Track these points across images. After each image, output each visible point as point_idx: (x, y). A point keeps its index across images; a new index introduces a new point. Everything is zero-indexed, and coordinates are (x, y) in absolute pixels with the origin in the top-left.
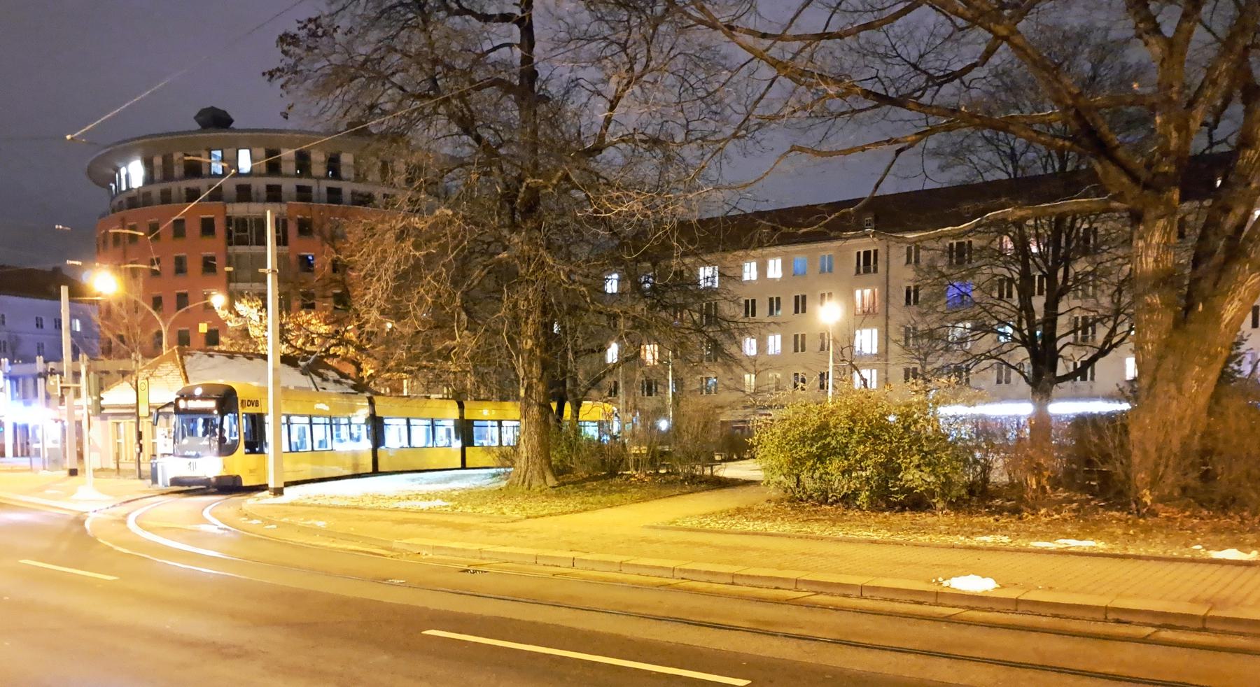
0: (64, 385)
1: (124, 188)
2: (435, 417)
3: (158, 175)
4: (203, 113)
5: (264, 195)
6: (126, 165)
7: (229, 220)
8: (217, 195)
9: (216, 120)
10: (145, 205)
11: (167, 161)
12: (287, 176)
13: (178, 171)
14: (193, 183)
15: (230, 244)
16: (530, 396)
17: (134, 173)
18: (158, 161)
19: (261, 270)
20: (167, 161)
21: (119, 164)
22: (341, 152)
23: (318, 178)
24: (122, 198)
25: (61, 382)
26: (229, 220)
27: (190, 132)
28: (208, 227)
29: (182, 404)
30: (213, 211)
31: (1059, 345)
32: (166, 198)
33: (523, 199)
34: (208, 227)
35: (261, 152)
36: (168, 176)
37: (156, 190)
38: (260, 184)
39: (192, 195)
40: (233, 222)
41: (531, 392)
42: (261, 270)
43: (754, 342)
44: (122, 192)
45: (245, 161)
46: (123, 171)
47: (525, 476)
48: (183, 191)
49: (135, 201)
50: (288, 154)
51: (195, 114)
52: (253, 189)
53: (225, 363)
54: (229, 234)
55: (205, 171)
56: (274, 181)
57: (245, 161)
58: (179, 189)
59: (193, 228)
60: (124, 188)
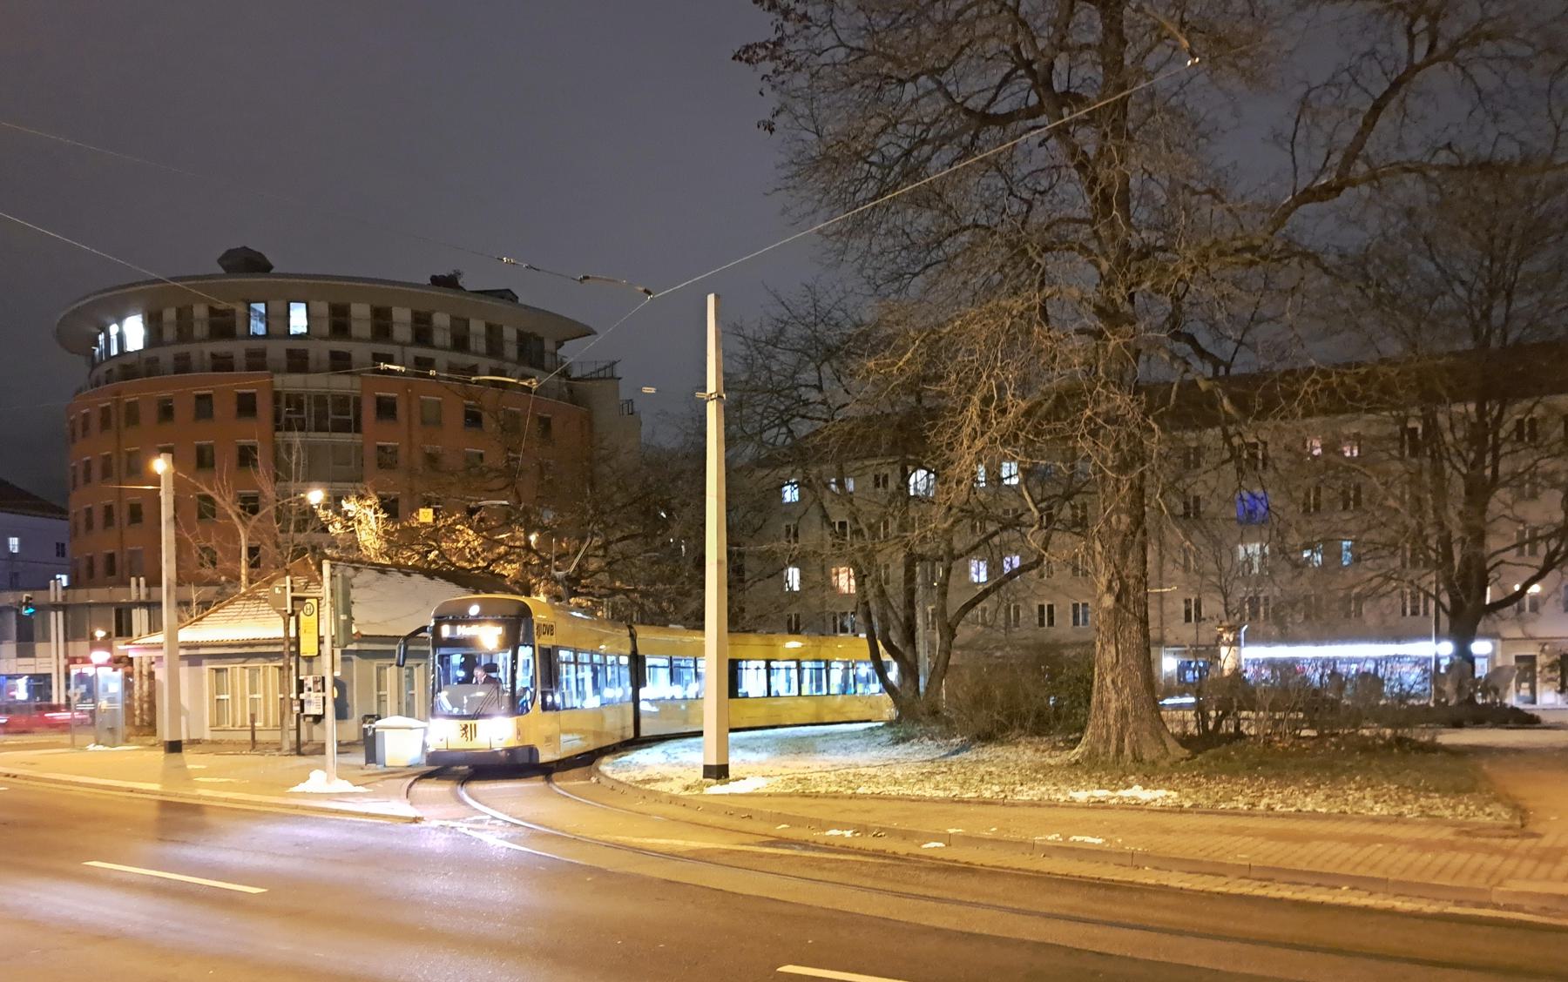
0: (294, 594)
1: (114, 351)
2: (829, 658)
3: (169, 333)
4: (230, 253)
5: (326, 364)
6: (119, 321)
7: (276, 397)
8: (257, 361)
9: (248, 262)
10: (149, 374)
11: (184, 315)
12: (359, 339)
13: (200, 330)
14: (222, 347)
15: (278, 429)
16: (1125, 607)
17: (133, 332)
18: (170, 315)
19: (699, 395)
20: (184, 315)
21: (108, 319)
22: (434, 311)
23: (403, 344)
24: (113, 365)
25: (293, 590)
26: (276, 397)
27: (210, 277)
28: (246, 406)
29: (446, 631)
30: (248, 383)
31: (1489, 565)
32: (183, 365)
33: (190, 475)
34: (246, 406)
35: (323, 308)
36: (184, 335)
37: (166, 355)
38: (320, 350)
39: (222, 364)
40: (284, 399)
41: (1128, 600)
42: (699, 395)
43: (983, 567)
44: (109, 357)
45: (298, 320)
46: (114, 329)
47: (1121, 739)
48: (207, 357)
49: (130, 367)
50: (360, 311)
51: (221, 252)
52: (312, 355)
53: (378, 580)
54: (277, 418)
55: (240, 329)
56: (339, 346)
57: (298, 320)
58: (202, 353)
59: (225, 408)
60: (114, 351)
